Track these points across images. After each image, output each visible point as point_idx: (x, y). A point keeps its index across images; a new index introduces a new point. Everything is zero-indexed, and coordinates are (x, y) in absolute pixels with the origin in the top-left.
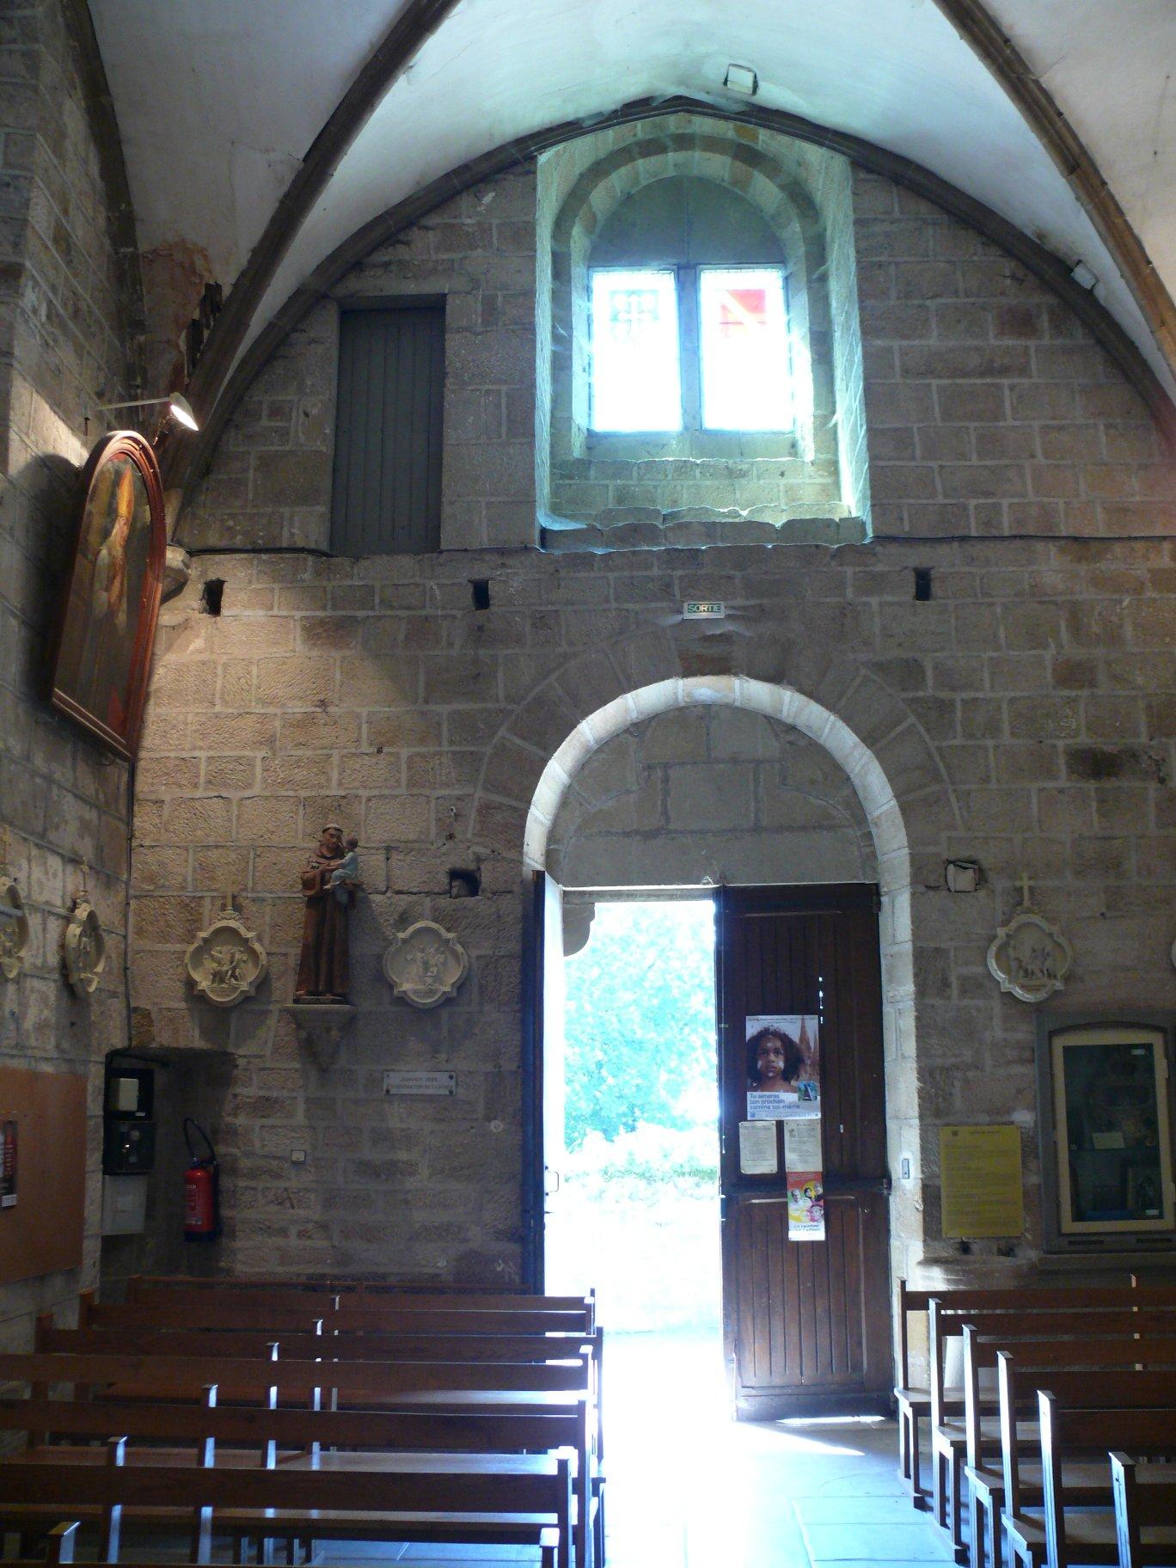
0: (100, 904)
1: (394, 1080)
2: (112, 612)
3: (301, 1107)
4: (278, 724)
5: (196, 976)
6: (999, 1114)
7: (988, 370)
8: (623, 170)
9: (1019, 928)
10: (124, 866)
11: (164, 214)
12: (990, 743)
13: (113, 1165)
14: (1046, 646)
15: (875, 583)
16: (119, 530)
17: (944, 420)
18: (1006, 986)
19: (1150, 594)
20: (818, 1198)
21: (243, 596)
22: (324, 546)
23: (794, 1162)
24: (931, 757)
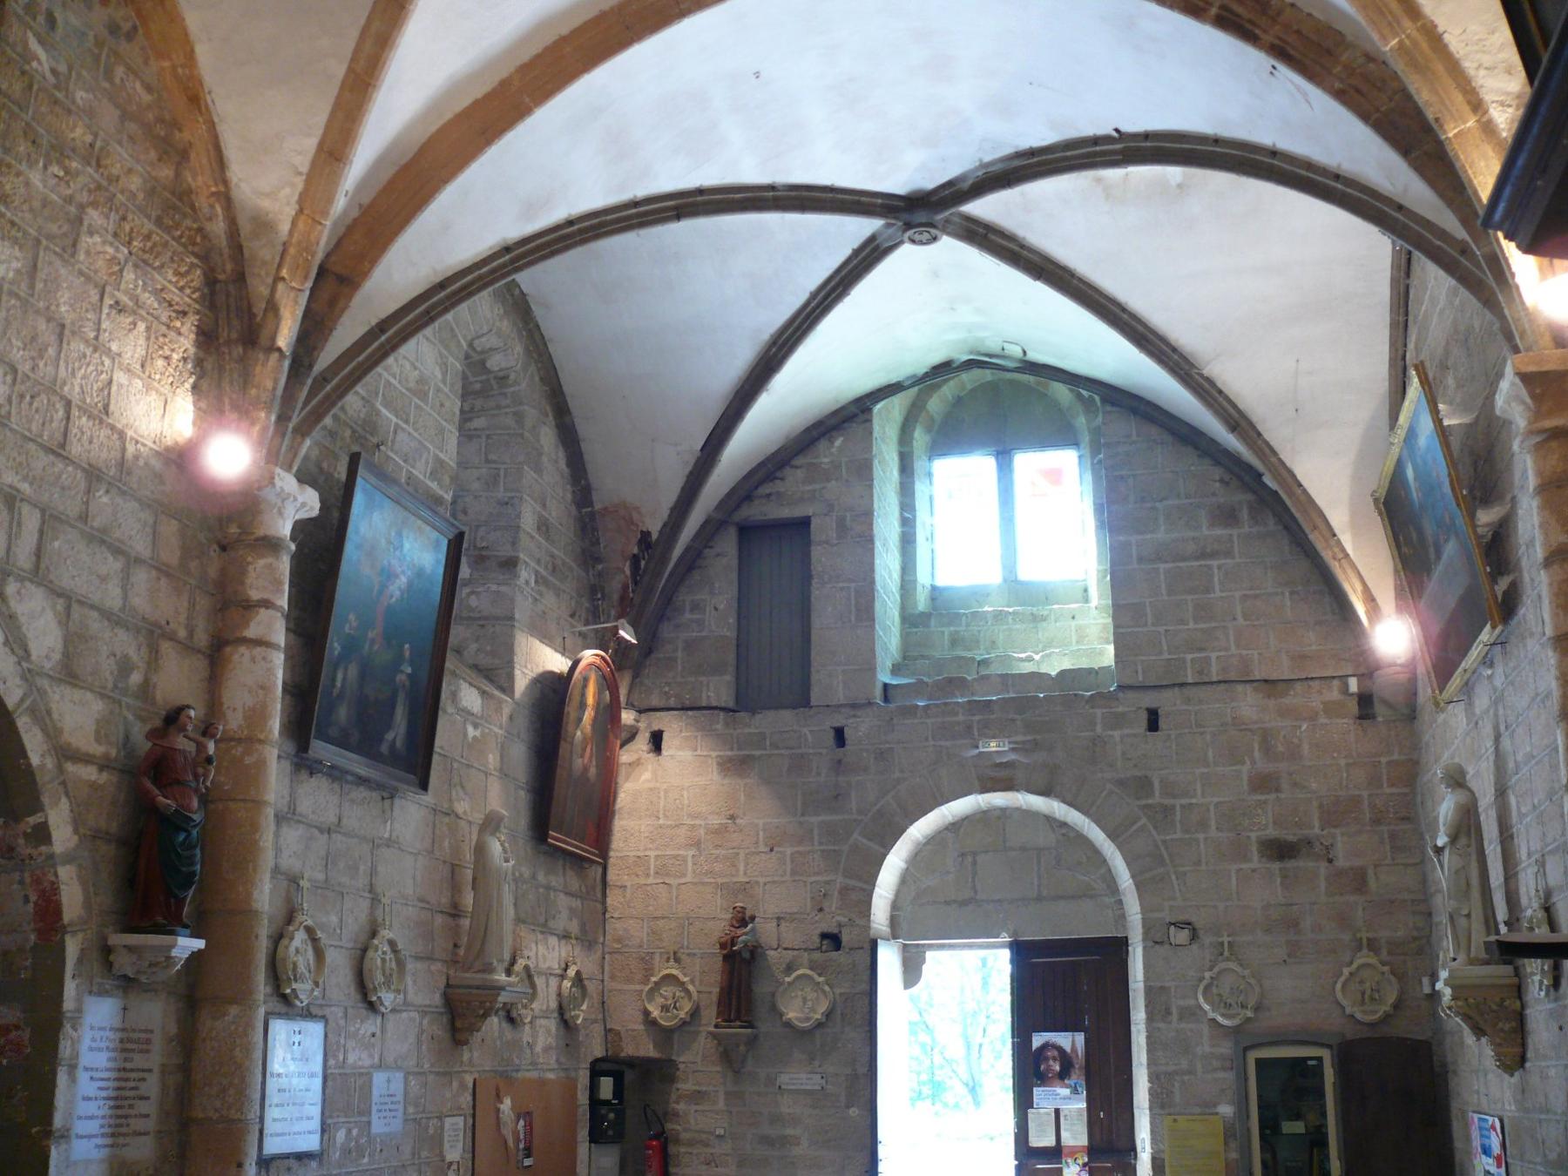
0: (585, 963)
1: (784, 1079)
2: (586, 769)
3: (722, 1096)
4: (702, 831)
5: (650, 1008)
6: (1208, 1107)
7: (1203, 555)
8: (951, 383)
9: (1220, 973)
10: (601, 931)
11: (609, 486)
12: (1201, 836)
13: (596, 1137)
14: (1243, 763)
15: (1117, 721)
16: (588, 715)
17: (1169, 595)
18: (1211, 1015)
19: (1323, 720)
20: (1085, 1165)
21: (676, 742)
22: (731, 704)
23: (1068, 1139)
24: (1157, 846)
